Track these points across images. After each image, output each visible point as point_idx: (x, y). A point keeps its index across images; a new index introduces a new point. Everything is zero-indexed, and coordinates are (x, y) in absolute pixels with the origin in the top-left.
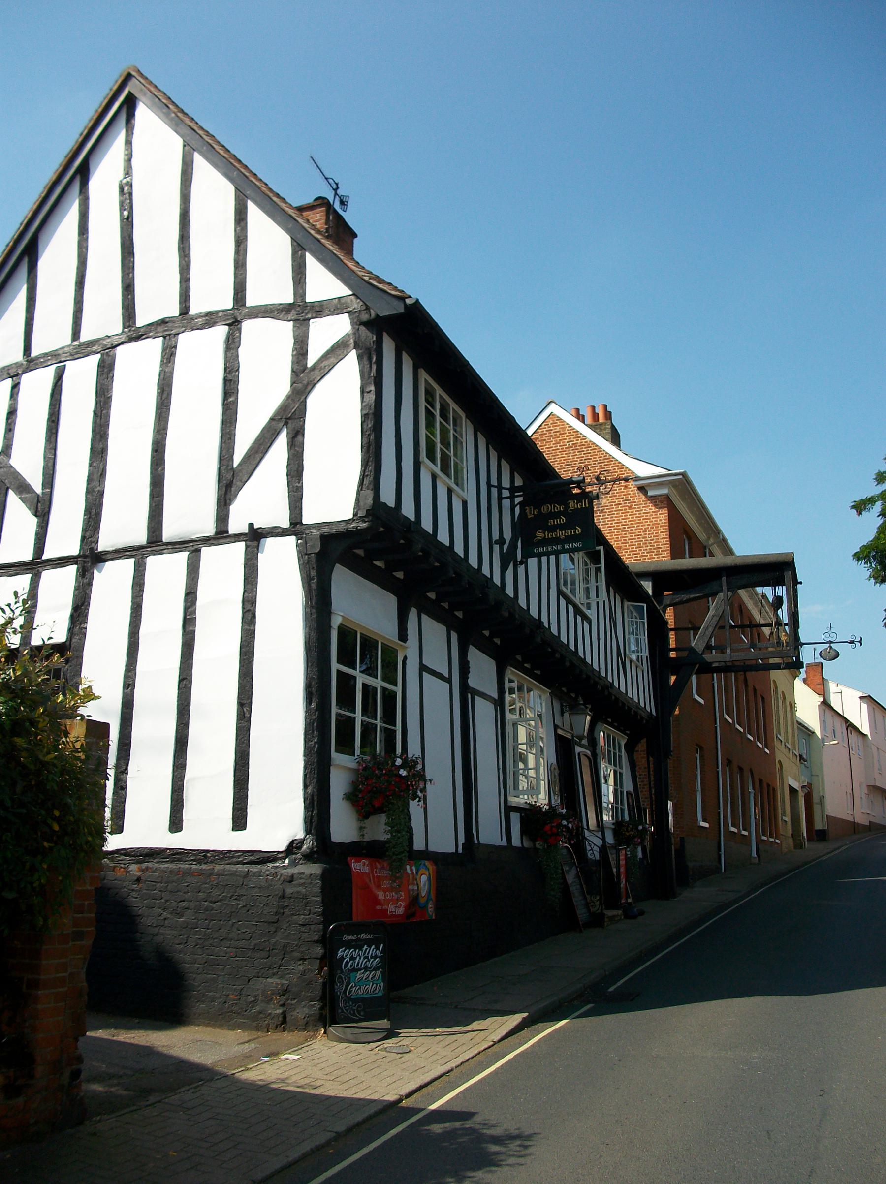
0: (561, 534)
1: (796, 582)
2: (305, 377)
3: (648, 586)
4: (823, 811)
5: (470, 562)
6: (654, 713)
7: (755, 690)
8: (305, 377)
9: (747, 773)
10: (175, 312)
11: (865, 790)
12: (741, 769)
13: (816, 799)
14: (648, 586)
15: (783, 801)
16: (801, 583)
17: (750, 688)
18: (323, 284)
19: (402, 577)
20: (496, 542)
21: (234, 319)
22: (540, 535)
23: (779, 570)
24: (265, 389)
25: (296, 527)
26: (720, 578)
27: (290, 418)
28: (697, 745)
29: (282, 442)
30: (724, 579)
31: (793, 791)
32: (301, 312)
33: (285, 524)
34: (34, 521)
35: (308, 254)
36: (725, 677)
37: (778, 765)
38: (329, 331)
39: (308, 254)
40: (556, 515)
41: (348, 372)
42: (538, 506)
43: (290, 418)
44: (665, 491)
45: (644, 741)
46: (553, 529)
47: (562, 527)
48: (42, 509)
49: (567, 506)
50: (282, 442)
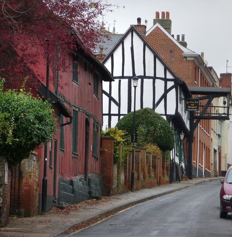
0: (193, 107)
2: (167, 91)
8: (167, 91)
10: (143, 75)
12: (202, 143)
15: (205, 158)
18: (169, 76)
21: (154, 78)
22: (189, 107)
24: (160, 92)
25: (166, 115)
26: (210, 94)
27: (164, 97)
29: (163, 100)
30: (211, 95)
32: (166, 80)
33: (164, 114)
34: (117, 107)
38: (170, 84)
40: (192, 104)
41: (173, 92)
42: (189, 101)
43: (164, 97)
44: (192, 59)
45: (186, 138)
46: (191, 106)
47: (193, 106)
48: (119, 105)
49: (194, 102)
50: (163, 100)
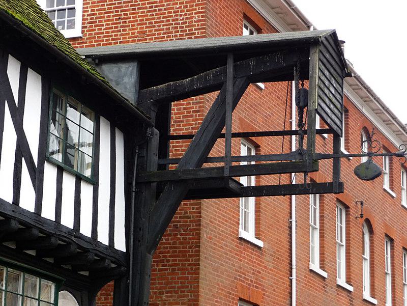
6: (120, 244)
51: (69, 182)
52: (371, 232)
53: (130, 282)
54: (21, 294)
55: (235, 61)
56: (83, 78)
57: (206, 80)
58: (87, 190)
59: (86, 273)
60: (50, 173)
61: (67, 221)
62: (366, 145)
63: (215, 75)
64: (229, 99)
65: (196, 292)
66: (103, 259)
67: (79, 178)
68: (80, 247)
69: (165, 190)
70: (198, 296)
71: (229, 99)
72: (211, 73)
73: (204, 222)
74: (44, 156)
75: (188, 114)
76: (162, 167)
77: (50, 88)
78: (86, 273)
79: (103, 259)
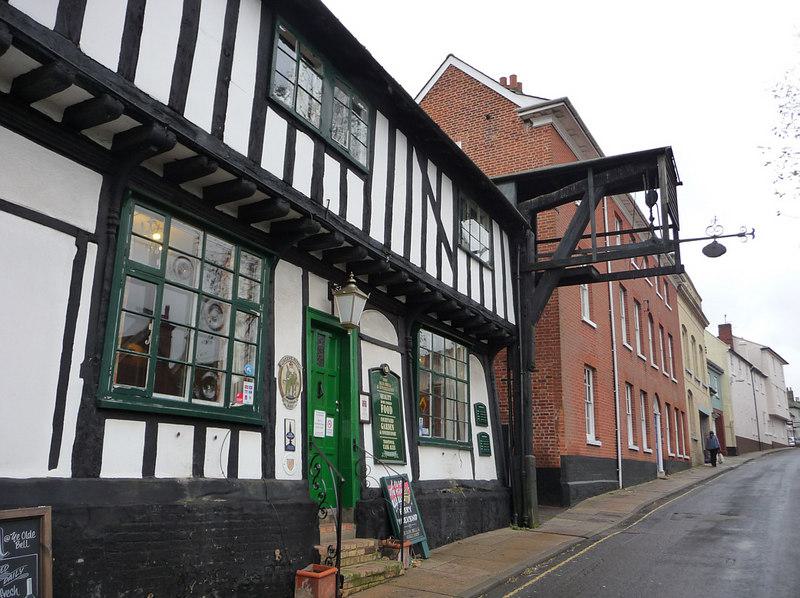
1: (674, 182)
3: (509, 192)
4: (732, 434)
5: (189, 114)
6: (512, 319)
7: (661, 327)
9: (651, 396)
11: (767, 418)
13: (726, 423)
14: (509, 192)
15: (693, 423)
16: (681, 184)
17: (656, 325)
19: (404, 301)
20: (670, 227)
23: (651, 169)
28: (586, 365)
30: (590, 180)
31: (703, 417)
35: (92, 97)
36: (590, 293)
37: (687, 394)
39: (92, 97)
51: (475, 267)
52: (652, 322)
53: (521, 347)
54: (227, 335)
55: (594, 174)
56: (483, 183)
57: (570, 191)
58: (487, 275)
59: (485, 342)
60: (462, 258)
61: (476, 297)
62: (645, 264)
63: (577, 187)
64: (592, 202)
65: (558, 358)
66: (500, 329)
67: (482, 265)
68: (485, 319)
69: (538, 279)
70: (560, 361)
71: (592, 202)
72: (573, 186)
73: (561, 307)
74: (457, 245)
75: (555, 222)
76: (536, 260)
77: (458, 190)
78: (485, 342)
79: (500, 329)
